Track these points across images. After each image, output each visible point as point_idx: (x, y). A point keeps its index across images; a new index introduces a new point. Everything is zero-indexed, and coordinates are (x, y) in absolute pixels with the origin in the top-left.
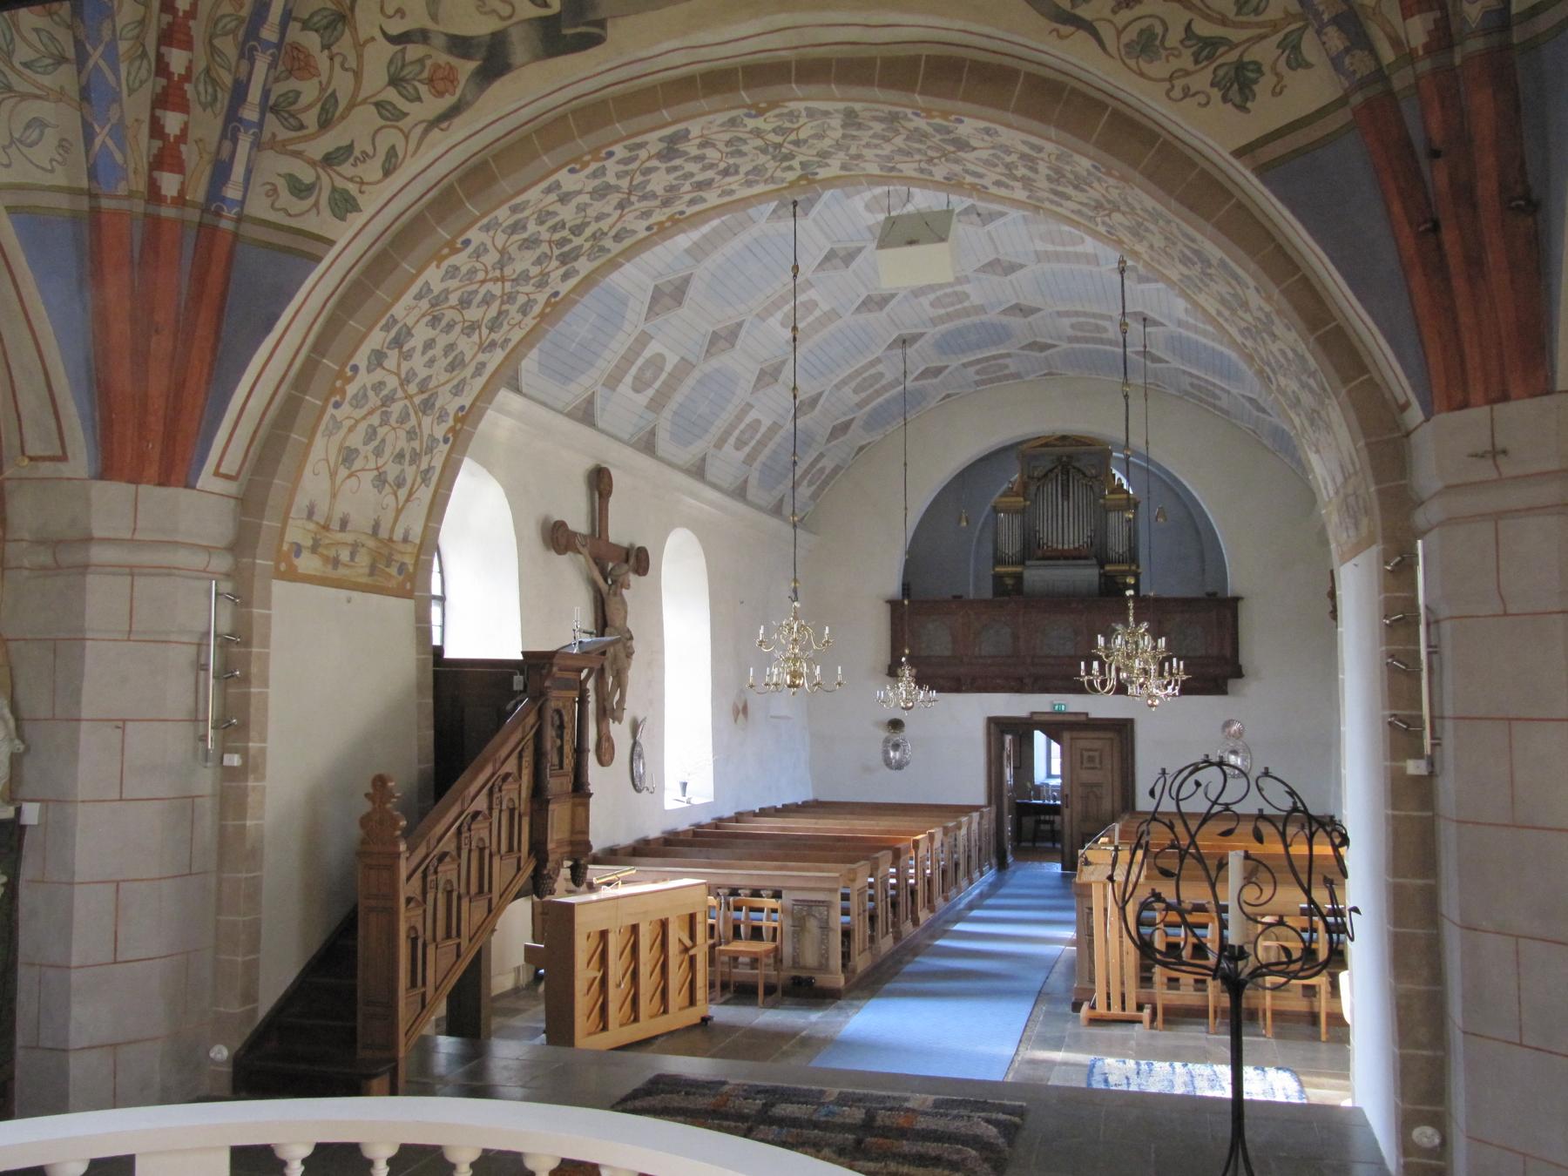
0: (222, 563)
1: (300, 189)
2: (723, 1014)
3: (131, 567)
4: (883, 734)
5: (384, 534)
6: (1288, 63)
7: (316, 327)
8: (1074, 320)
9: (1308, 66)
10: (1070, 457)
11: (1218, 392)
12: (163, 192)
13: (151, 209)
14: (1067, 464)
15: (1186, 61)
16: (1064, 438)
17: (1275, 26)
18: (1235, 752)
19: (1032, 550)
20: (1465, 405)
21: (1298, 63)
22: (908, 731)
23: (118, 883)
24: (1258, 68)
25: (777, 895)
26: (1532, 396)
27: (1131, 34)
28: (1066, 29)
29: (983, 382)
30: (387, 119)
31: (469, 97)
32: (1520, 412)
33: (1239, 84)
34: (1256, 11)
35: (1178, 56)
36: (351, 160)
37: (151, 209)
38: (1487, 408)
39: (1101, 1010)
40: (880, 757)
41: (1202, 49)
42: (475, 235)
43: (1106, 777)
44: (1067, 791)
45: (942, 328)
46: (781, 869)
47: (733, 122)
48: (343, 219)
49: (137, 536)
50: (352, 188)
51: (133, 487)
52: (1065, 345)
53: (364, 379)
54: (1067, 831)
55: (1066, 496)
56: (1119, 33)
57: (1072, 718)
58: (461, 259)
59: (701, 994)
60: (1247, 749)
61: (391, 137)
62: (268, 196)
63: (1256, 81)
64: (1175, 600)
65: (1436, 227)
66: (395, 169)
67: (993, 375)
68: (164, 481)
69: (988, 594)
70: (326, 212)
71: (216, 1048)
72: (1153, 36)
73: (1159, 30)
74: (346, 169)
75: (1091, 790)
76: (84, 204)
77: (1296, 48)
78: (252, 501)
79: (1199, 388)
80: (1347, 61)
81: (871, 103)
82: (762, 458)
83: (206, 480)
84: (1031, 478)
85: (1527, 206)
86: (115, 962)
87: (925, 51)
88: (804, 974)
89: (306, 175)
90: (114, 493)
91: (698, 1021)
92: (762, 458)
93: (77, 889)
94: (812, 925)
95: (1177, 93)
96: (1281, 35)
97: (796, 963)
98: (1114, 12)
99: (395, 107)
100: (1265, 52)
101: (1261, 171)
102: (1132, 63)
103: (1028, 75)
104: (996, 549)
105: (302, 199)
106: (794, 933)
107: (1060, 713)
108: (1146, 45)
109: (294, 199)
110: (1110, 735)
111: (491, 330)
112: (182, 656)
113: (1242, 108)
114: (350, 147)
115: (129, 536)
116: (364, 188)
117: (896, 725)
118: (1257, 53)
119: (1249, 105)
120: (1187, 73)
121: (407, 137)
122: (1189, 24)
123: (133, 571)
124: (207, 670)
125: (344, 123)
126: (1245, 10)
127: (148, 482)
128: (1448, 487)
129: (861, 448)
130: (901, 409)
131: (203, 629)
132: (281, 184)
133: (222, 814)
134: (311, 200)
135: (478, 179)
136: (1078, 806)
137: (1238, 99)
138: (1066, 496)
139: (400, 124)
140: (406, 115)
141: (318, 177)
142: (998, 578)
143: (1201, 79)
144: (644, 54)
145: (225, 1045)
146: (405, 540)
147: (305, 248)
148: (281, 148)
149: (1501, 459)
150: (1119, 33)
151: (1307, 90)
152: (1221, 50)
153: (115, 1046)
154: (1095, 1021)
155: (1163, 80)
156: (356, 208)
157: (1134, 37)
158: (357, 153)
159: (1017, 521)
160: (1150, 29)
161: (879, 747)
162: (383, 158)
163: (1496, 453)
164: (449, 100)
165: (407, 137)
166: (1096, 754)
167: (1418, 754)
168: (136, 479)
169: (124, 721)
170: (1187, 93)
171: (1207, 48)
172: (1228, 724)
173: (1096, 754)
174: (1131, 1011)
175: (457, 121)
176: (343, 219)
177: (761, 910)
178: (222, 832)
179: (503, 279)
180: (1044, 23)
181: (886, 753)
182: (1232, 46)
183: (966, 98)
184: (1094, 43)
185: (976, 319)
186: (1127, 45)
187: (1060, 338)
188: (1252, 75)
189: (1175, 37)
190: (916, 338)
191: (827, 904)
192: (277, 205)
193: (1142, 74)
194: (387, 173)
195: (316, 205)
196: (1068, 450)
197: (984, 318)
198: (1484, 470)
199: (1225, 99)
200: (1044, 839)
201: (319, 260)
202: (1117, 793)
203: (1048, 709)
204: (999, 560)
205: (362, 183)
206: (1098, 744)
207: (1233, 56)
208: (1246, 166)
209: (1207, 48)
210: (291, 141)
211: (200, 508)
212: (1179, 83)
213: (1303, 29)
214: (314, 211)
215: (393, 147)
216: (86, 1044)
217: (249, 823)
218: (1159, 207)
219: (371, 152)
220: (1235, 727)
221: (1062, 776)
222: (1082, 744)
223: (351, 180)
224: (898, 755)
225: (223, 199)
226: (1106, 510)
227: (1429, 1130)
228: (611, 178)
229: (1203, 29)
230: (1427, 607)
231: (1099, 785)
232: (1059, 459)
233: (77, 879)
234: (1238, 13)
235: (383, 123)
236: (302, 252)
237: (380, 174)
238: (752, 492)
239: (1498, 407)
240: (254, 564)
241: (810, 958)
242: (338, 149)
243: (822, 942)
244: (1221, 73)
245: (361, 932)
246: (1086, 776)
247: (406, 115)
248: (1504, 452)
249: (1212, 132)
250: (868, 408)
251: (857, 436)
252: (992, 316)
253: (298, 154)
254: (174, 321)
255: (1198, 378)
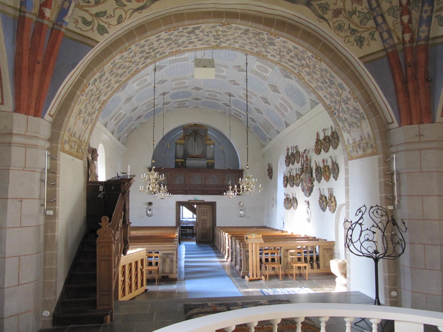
0: (48, 145)
1: (86, 23)
2: (151, 288)
3: (24, 144)
4: (146, 206)
5: (81, 139)
6: (371, 39)
7: (83, 69)
8: (210, 93)
9: (376, 40)
10: (197, 130)
11: (242, 115)
12: (46, 15)
13: (40, 20)
14: (195, 132)
15: (348, 33)
16: (196, 125)
17: (368, 29)
18: (241, 210)
19: (186, 156)
20: (411, 124)
21: (373, 38)
22: (153, 205)
23: (19, 256)
24: (364, 38)
25: (158, 253)
26: (429, 123)
27: (336, 24)
28: (322, 20)
29: (178, 107)
30: (119, 6)
31: (148, 4)
32: (426, 127)
33: (360, 41)
34: (364, 25)
35: (347, 32)
36: (106, 16)
37: (40, 20)
38: (418, 125)
39: (251, 277)
40: (145, 213)
41: (352, 31)
42: (133, 47)
43: (208, 217)
44: (198, 222)
45: (175, 91)
46: (151, 245)
47: (214, 27)
48: (102, 35)
49: (27, 134)
50: (106, 26)
51: (26, 116)
52: (204, 99)
53: (90, 87)
54: (197, 233)
55: (195, 141)
56: (334, 23)
57: (200, 202)
58: (125, 54)
59: (145, 282)
60: (244, 210)
61: (119, 12)
62: (75, 23)
63: (364, 42)
64: (219, 170)
65: (407, 83)
66: (121, 22)
67: (181, 106)
68: (36, 115)
69: (173, 166)
70: (96, 31)
71: (45, 312)
72: (341, 26)
73: (343, 25)
74: (104, 19)
75: (204, 221)
76: (17, 14)
77: (373, 35)
78: (57, 124)
79: (236, 114)
80: (388, 41)
81: (252, 28)
82: (119, 124)
83: (47, 117)
84: (186, 135)
85: (429, 81)
86: (19, 285)
87: (276, 17)
88: (165, 275)
89: (89, 19)
90: (19, 118)
91: (144, 291)
92: (119, 124)
93: (7, 260)
94: (168, 260)
95: (346, 41)
96: (369, 32)
97: (163, 272)
98: (333, 18)
99: (122, 3)
100: (366, 35)
101: (365, 63)
102: (336, 32)
103: (303, 30)
104: (176, 154)
105: (87, 26)
106: (162, 263)
107: (196, 200)
108: (340, 28)
109: (84, 26)
110: (209, 206)
111: (120, 77)
112: (38, 176)
113: (361, 47)
114: (105, 12)
115: (24, 133)
116: (110, 26)
117: (150, 204)
118: (364, 35)
119: (362, 47)
120: (349, 37)
121: (126, 13)
122: (349, 25)
123: (25, 146)
124: (44, 182)
125: (104, 4)
126: (362, 24)
127: (31, 115)
128: (406, 143)
129: (142, 123)
130: (154, 112)
131: (44, 168)
132: (80, 20)
133: (46, 232)
134: (91, 27)
135: (141, 30)
136: (200, 226)
137: (360, 45)
138: (195, 141)
139: (124, 8)
140: (126, 6)
141: (93, 20)
142: (176, 163)
143: (352, 39)
144: (203, 2)
145: (48, 310)
146: (84, 141)
147: (84, 41)
148: (81, 8)
149: (421, 137)
150: (334, 23)
151: (376, 46)
152: (356, 32)
153: (18, 315)
154: (250, 280)
155: (343, 37)
156: (107, 32)
157: (337, 25)
158: (108, 14)
159: (182, 147)
160: (341, 24)
161: (145, 210)
162: (118, 18)
163: (420, 135)
164: (141, 4)
165: (126, 13)
166: (206, 211)
167: (393, 204)
168: (27, 114)
169: (21, 199)
170: (349, 42)
171: (353, 31)
172: (240, 203)
173: (206, 211)
174: (259, 277)
175: (144, 11)
176: (102, 35)
177: (152, 257)
178: (46, 237)
179: (130, 62)
180: (317, 18)
181: (147, 212)
182: (359, 32)
183: (287, 32)
184: (327, 24)
185: (184, 90)
186: (336, 27)
187: (204, 97)
188: (363, 40)
189: (346, 27)
190: (167, 93)
191: (172, 254)
192: (78, 26)
193: (338, 35)
194: (119, 23)
195: (92, 28)
196: (196, 128)
197: (186, 90)
198: (417, 139)
199: (357, 44)
200: (184, 236)
201: (93, 47)
202: (211, 222)
203: (193, 199)
204: (176, 157)
205: (109, 24)
206: (206, 209)
207: (359, 35)
208: (361, 62)
209: (353, 31)
210: (85, 6)
211: (43, 125)
212: (347, 39)
213: (375, 32)
214: (91, 31)
215: (121, 15)
216: (9, 316)
217: (56, 234)
218: (327, 68)
219: (113, 15)
220: (242, 204)
221: (196, 218)
222: (202, 209)
223: (106, 23)
224: (151, 212)
225: (64, 21)
226: (206, 145)
227: (395, 292)
228: (172, 37)
229: (353, 27)
230: (396, 171)
231: (206, 220)
232: (194, 130)
233: (7, 256)
234: (360, 24)
235: (118, 7)
236: (87, 44)
237: (116, 23)
238: (115, 133)
239: (421, 125)
240: (57, 146)
241: (167, 270)
242: (101, 12)
243: (171, 265)
244: (356, 38)
245: (98, 268)
246: (203, 217)
247: (126, 6)
248: (422, 135)
249: (352, 53)
250: (147, 112)
251: (142, 120)
252: (189, 90)
253: (87, 11)
254: (43, 59)
255: (238, 111)
